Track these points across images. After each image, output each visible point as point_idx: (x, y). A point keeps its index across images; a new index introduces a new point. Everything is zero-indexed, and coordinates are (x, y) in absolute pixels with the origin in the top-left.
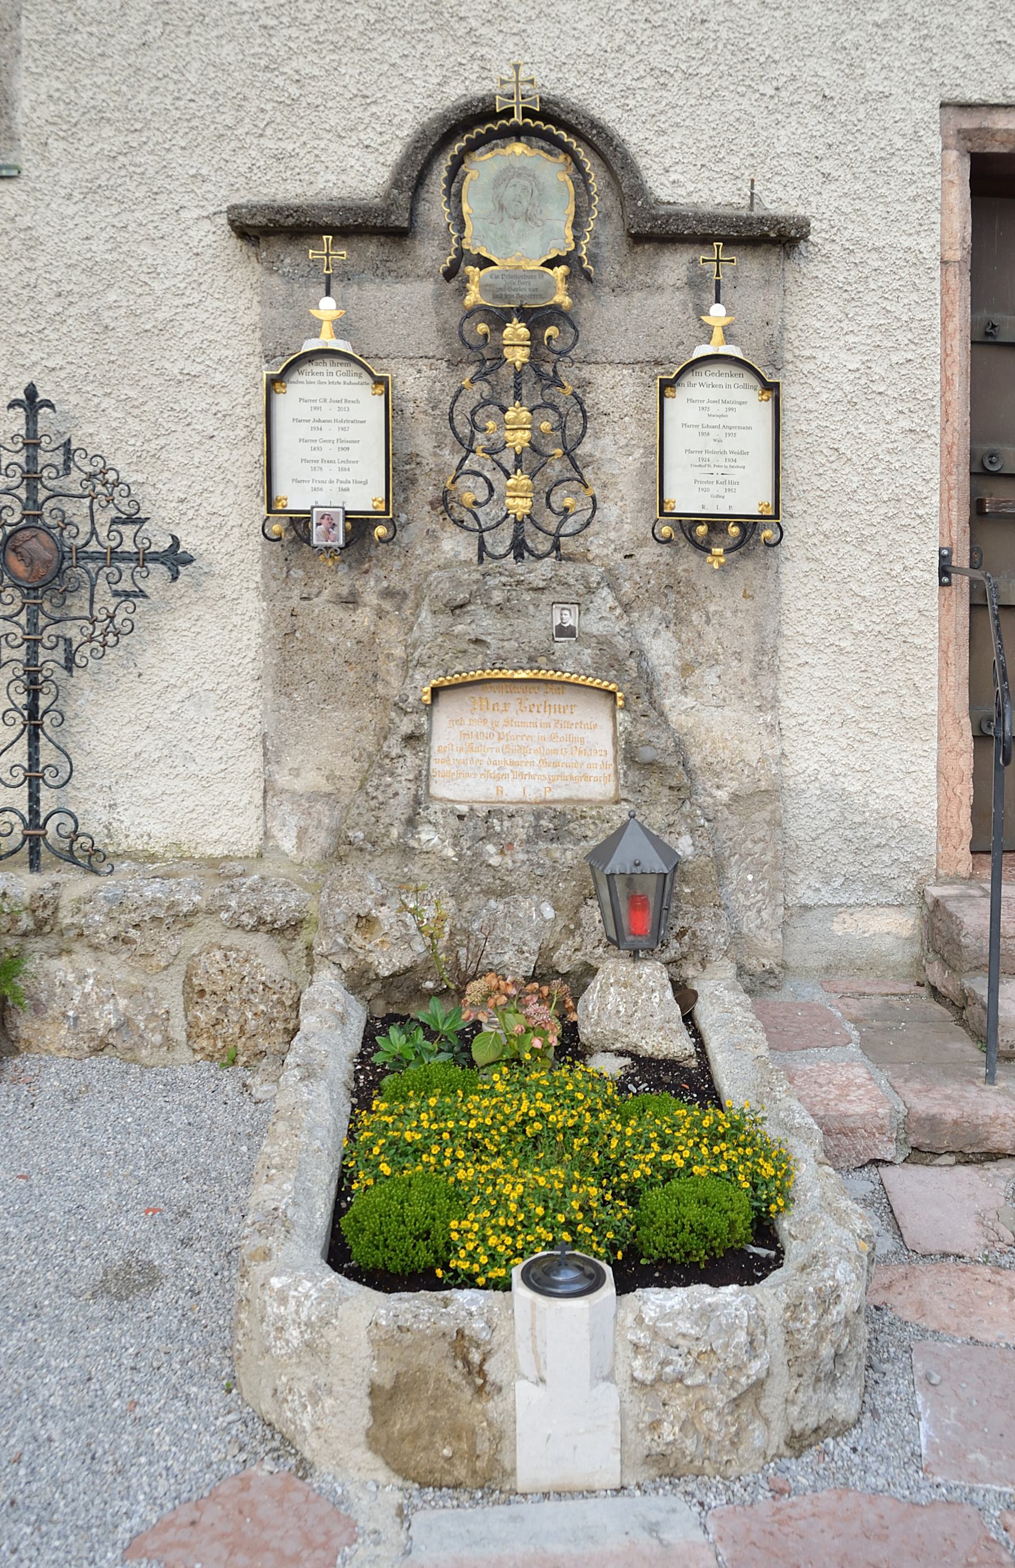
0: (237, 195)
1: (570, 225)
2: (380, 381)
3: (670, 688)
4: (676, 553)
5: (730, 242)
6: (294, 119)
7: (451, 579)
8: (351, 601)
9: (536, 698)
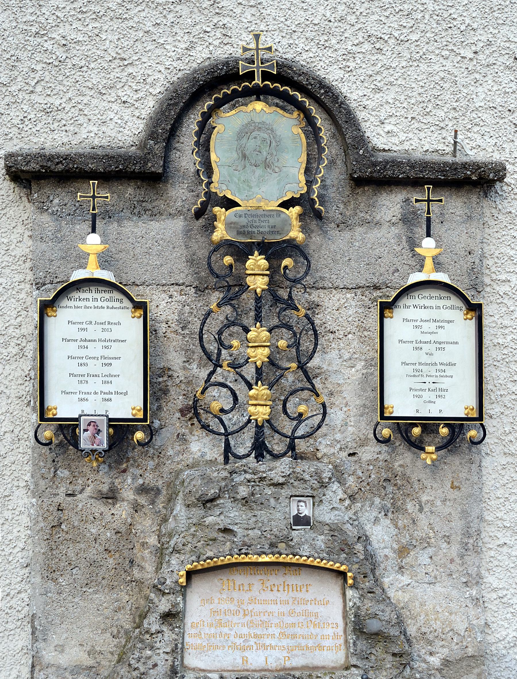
0: (10, 143)
1: (303, 171)
2: (140, 306)
3: (389, 568)
4: (393, 451)
5: (439, 184)
6: (61, 78)
7: (203, 476)
8: (111, 496)
9: (276, 579)
